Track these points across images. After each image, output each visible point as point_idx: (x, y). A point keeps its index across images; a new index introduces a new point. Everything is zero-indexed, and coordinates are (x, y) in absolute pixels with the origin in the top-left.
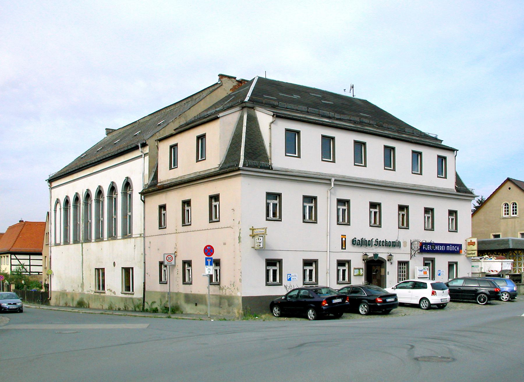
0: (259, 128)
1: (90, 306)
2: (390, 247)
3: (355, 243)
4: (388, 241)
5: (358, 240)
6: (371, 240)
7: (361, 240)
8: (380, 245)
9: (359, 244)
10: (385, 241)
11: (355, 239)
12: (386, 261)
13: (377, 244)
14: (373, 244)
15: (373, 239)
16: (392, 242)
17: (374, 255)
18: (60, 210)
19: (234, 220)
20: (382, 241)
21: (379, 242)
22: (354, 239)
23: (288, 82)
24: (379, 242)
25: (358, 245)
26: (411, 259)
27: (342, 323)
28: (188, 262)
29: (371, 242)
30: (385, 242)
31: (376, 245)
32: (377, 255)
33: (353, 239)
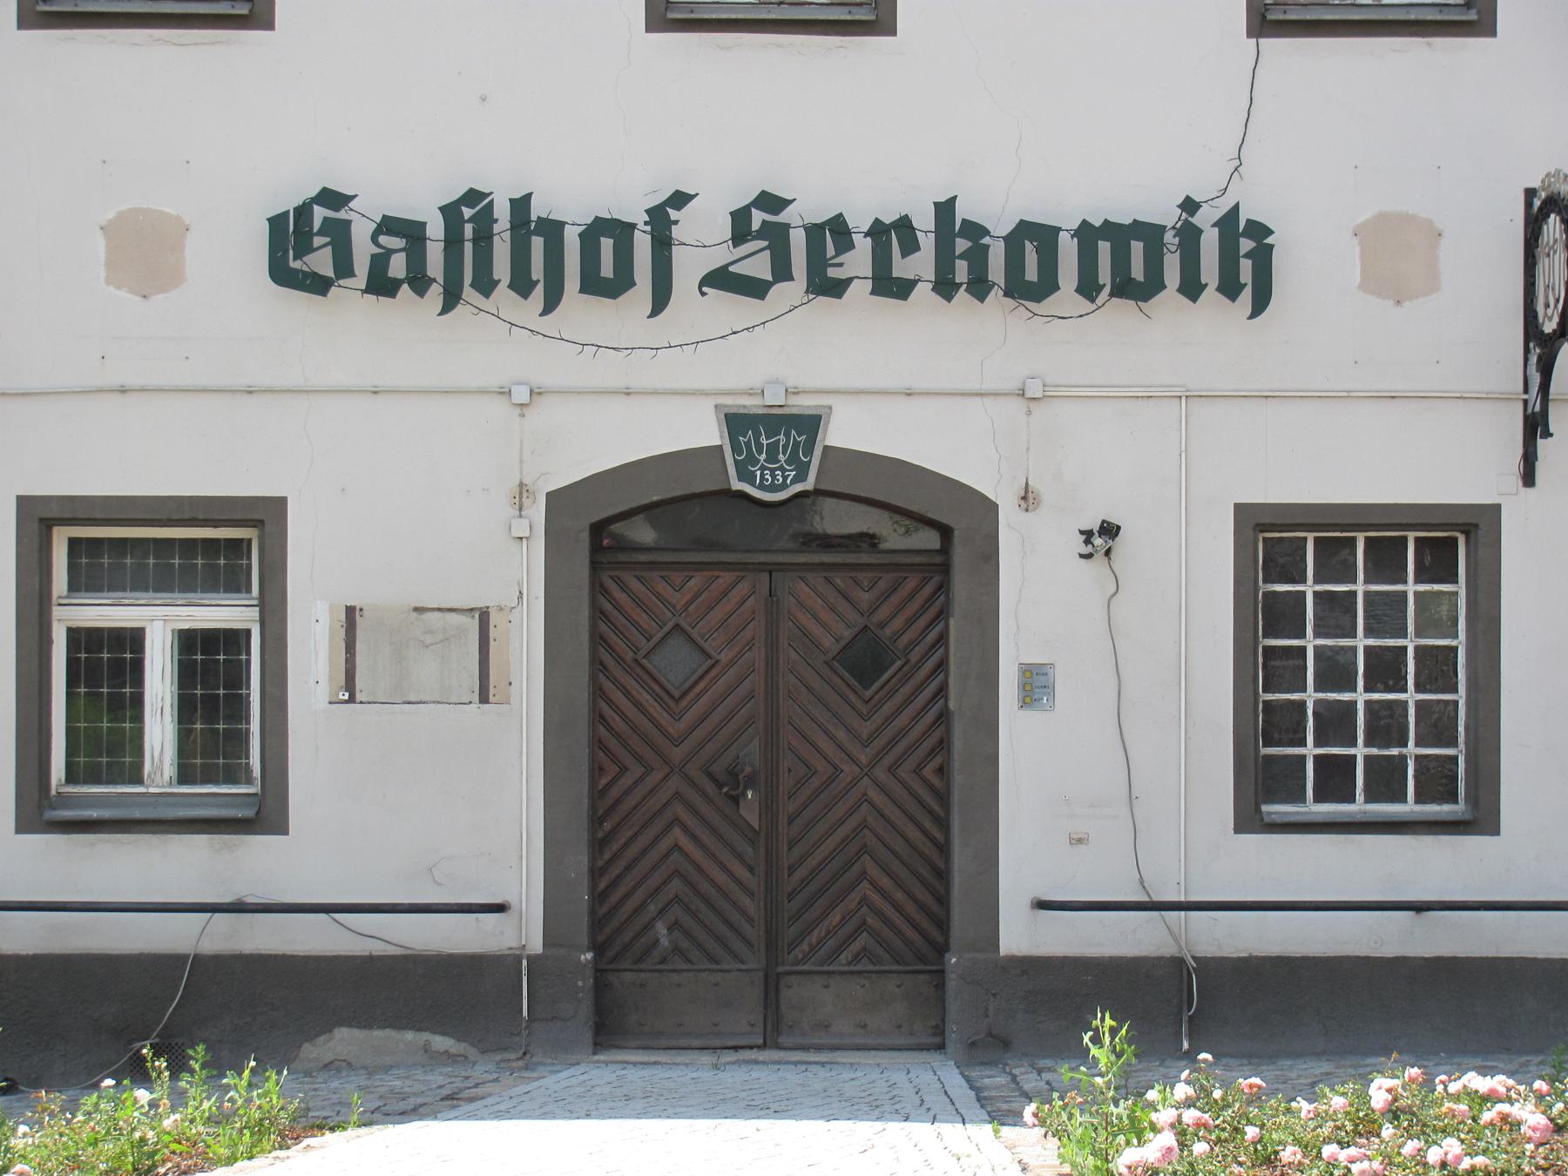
0: (354, 958)
1: (1410, 1141)
2: (1051, 304)
3: (321, 261)
4: (1001, 226)
5: (389, 225)
6: (640, 218)
7: (436, 229)
8: (836, 288)
9: (398, 267)
10: (924, 221)
11: (320, 213)
12: (993, 508)
13: (759, 267)
14: (688, 267)
15: (680, 199)
16: (1087, 234)
17: (736, 423)
18: (1014, 385)
19: (484, 99)
20: (878, 231)
21: (798, 239)
22: (303, 211)
23: (54, 646)
24: (798, 239)
25: (381, 285)
26: (1529, 478)
27: (956, 823)
28: (949, 738)
29: (642, 245)
30: (927, 242)
31: (755, 289)
32: (810, 424)
33: (289, 203)
